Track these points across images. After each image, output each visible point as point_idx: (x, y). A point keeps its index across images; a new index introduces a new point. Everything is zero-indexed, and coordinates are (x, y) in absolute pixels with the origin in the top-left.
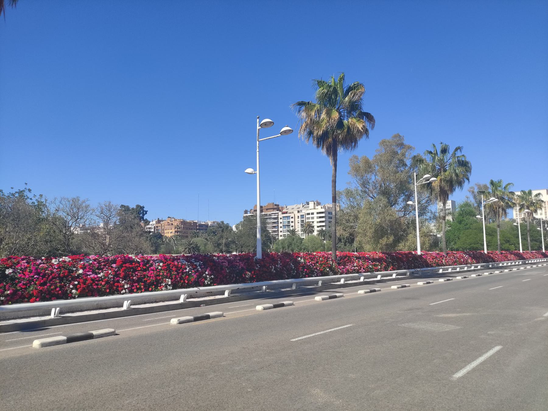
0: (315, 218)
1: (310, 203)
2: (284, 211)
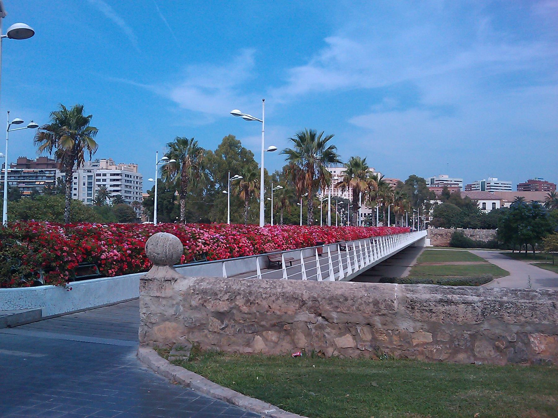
0: (108, 181)
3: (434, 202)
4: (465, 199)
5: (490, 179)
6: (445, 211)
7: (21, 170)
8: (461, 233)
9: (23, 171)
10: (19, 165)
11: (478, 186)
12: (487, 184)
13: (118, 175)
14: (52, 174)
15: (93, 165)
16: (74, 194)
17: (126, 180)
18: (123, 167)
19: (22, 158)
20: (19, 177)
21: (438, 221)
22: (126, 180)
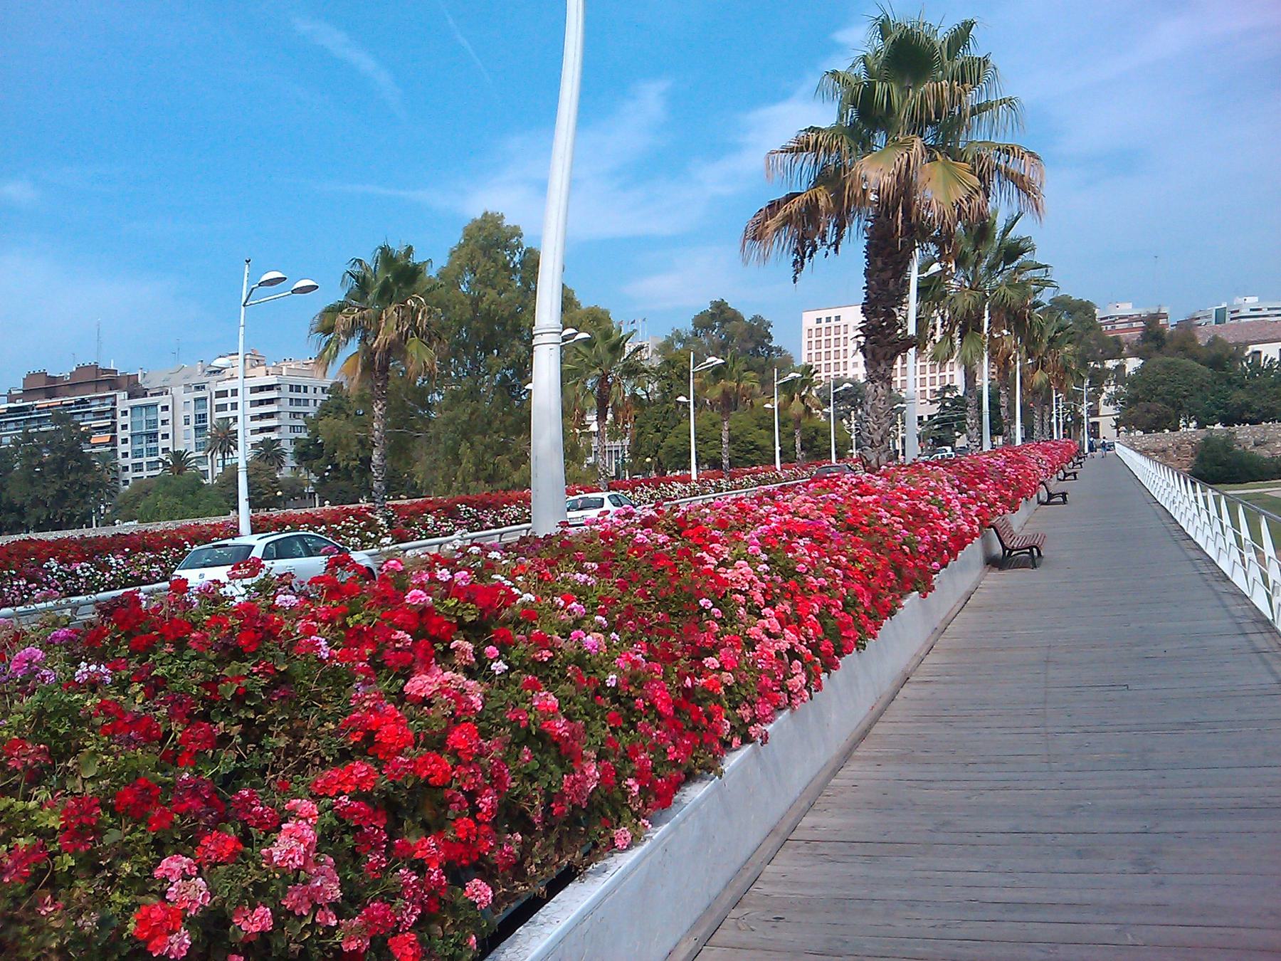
3: (1117, 363)
4: (1210, 344)
5: (1240, 300)
6: (1163, 382)
7: (31, 403)
8: (1227, 440)
9: (36, 405)
10: (28, 393)
11: (1207, 320)
12: (1232, 312)
13: (270, 388)
14: (108, 404)
15: (211, 372)
16: (163, 449)
17: (291, 399)
18: (284, 368)
19: (34, 374)
20: (27, 421)
21: (1148, 411)
22: (291, 399)
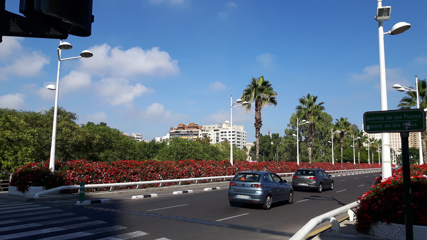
0: (236, 136)
1: (223, 124)
2: (203, 129)
17: (237, 135)
22: (237, 135)
